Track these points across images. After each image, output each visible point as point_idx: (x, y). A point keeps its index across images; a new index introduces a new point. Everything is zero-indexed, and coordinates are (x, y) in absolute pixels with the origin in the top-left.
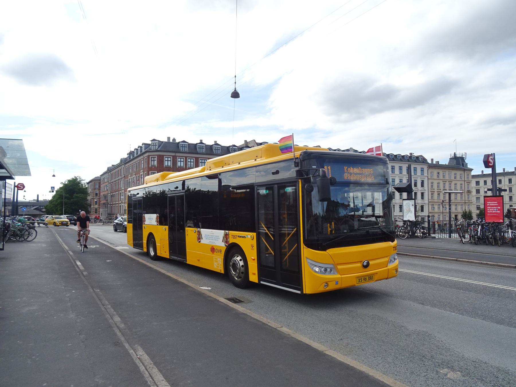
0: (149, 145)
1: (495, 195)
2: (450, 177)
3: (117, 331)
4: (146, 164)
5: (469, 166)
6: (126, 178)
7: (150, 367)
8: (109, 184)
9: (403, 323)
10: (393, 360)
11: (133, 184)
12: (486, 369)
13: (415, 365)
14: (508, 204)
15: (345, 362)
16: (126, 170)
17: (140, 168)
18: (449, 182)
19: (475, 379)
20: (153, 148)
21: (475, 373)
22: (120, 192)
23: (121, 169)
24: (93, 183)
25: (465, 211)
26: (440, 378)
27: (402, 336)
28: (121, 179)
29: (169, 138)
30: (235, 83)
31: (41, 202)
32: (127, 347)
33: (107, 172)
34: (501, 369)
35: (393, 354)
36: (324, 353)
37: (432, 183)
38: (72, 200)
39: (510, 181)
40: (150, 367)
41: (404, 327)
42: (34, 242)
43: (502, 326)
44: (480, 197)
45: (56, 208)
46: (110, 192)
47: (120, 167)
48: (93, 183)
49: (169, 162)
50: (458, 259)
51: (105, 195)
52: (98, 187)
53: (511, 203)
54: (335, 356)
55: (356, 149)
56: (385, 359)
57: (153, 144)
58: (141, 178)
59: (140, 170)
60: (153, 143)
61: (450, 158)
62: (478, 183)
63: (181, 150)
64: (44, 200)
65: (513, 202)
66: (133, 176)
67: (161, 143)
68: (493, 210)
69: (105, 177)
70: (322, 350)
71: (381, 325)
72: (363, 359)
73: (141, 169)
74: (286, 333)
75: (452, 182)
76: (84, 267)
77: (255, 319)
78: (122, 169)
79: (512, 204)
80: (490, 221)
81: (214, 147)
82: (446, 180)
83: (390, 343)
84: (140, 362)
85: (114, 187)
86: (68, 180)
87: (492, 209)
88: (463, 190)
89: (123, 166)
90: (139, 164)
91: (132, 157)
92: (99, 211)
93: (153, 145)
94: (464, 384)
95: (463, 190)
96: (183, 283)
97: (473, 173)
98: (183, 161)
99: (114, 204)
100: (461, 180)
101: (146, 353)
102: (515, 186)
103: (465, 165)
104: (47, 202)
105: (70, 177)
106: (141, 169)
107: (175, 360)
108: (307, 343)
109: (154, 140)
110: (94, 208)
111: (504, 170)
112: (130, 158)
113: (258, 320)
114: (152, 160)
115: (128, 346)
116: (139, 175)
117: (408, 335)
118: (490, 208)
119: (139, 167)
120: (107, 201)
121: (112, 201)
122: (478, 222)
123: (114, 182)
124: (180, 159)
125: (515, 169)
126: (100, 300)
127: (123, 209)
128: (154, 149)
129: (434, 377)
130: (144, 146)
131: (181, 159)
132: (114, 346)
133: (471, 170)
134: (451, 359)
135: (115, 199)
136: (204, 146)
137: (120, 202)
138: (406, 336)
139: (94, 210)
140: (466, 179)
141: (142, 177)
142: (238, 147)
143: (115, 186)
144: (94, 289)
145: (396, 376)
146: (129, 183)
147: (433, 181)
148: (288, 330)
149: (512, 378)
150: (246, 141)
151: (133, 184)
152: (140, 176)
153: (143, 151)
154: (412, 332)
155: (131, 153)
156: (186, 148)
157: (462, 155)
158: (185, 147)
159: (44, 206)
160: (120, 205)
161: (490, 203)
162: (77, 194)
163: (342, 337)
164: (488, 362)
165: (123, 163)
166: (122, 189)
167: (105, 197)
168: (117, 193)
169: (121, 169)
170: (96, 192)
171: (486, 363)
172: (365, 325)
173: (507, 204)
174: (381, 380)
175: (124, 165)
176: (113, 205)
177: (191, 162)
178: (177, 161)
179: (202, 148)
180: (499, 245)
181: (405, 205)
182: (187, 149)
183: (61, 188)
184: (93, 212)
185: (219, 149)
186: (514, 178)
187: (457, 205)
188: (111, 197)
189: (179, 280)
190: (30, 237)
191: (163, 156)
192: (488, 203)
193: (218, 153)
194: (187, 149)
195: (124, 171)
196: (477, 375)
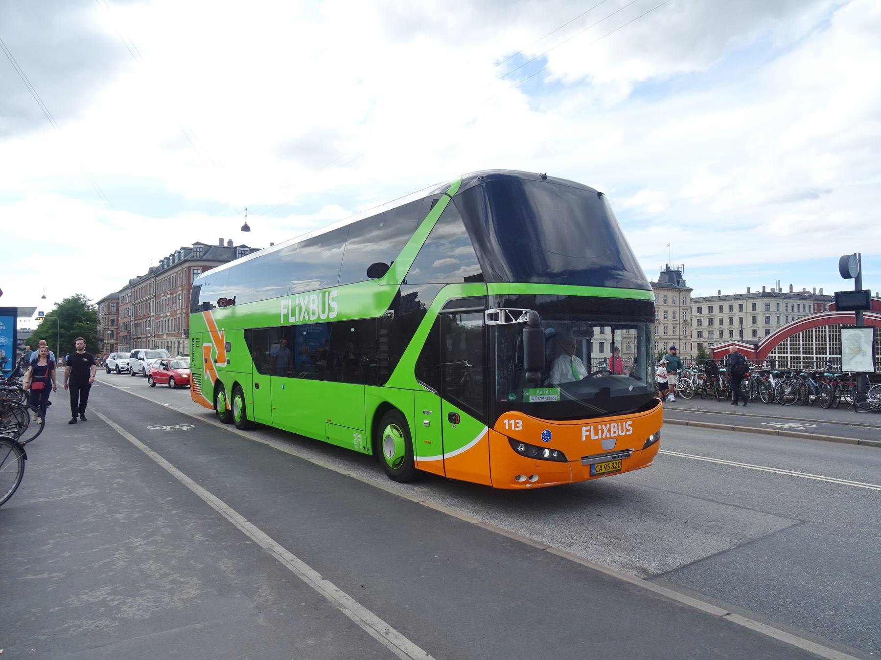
0: (190, 249)
5: (688, 285)
6: (157, 298)
11: (167, 309)
22: (149, 319)
24: (107, 303)
28: (150, 299)
29: (222, 240)
33: (128, 287)
38: (71, 331)
44: (713, 331)
48: (107, 303)
50: (690, 422)
58: (178, 300)
60: (197, 248)
62: (711, 309)
67: (209, 248)
73: (178, 286)
79: (702, 342)
86: (65, 300)
88: (677, 321)
89: (153, 280)
93: (197, 251)
95: (677, 321)
96: (436, 512)
97: (693, 295)
99: (139, 338)
100: (665, 306)
104: (26, 332)
105: (69, 294)
106: (178, 286)
109: (197, 244)
110: (108, 344)
111: (804, 289)
112: (163, 269)
114: (194, 274)
116: (175, 295)
119: (177, 283)
120: (129, 332)
121: (136, 333)
123: (140, 303)
133: (690, 290)
135: (141, 330)
137: (149, 335)
139: (108, 347)
140: (681, 304)
143: (142, 310)
151: (167, 309)
160: (148, 339)
167: (126, 326)
168: (143, 320)
170: (112, 318)
176: (139, 340)
181: (845, 340)
183: (54, 312)
184: (107, 351)
187: (668, 343)
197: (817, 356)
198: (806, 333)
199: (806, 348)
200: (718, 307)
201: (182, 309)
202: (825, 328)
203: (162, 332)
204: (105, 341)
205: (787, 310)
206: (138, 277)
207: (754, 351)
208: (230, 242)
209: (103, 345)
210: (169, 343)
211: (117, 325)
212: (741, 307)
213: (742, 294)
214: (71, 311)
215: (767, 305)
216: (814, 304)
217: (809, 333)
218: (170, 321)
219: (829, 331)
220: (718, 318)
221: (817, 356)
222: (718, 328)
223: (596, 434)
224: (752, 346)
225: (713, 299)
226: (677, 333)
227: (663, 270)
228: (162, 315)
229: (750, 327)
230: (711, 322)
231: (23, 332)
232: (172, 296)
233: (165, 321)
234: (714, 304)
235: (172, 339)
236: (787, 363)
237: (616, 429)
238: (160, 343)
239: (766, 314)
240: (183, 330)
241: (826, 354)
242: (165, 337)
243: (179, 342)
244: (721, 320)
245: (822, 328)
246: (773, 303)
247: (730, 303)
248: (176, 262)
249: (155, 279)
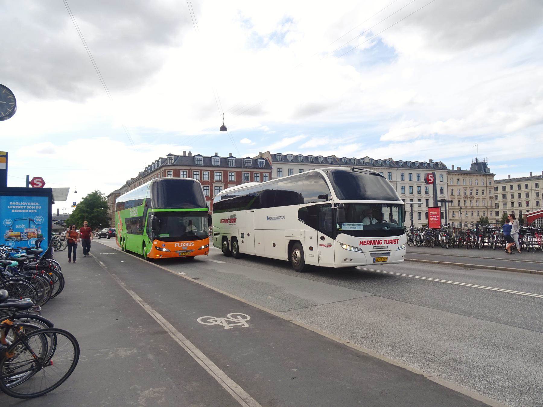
0: (166, 159)
1: (435, 206)
2: (471, 183)
5: (491, 172)
14: (518, 209)
18: (470, 188)
20: (168, 162)
25: (482, 218)
29: (184, 152)
30: (223, 119)
31: (62, 216)
33: (126, 186)
37: (452, 190)
39: (537, 185)
42: (65, 251)
44: (506, 203)
45: (78, 222)
53: (497, 210)
54: (227, 294)
55: (372, 158)
61: (472, 163)
62: (504, 188)
63: (197, 164)
64: (64, 214)
67: (177, 157)
68: (434, 218)
75: (473, 188)
82: (466, 187)
86: (89, 194)
97: (496, 178)
102: (542, 190)
103: (487, 170)
104: (67, 216)
105: (91, 191)
109: (170, 155)
114: (168, 174)
125: (542, 173)
128: (170, 163)
133: (494, 175)
136: (219, 159)
147: (459, 188)
150: (260, 153)
156: (201, 161)
158: (200, 160)
159: (65, 220)
161: (432, 212)
162: (98, 208)
173: (534, 209)
177: (206, 175)
178: (193, 174)
179: (217, 161)
180: (479, 248)
182: (202, 163)
183: (81, 203)
186: (541, 183)
190: (62, 247)
191: (179, 170)
192: (431, 212)
194: (202, 163)
200: (525, 185)
204: (112, 220)
206: (132, 179)
208: (190, 153)
209: (111, 222)
212: (527, 186)
213: (505, 180)
214: (91, 201)
220: (525, 193)
222: (518, 200)
223: (180, 245)
225: (506, 181)
226: (486, 205)
227: (473, 162)
229: (534, 200)
230: (504, 197)
231: (65, 216)
234: (498, 185)
237: (187, 244)
239: (503, 193)
244: (512, 196)
247: (519, 183)
248: (149, 172)
249: (143, 180)
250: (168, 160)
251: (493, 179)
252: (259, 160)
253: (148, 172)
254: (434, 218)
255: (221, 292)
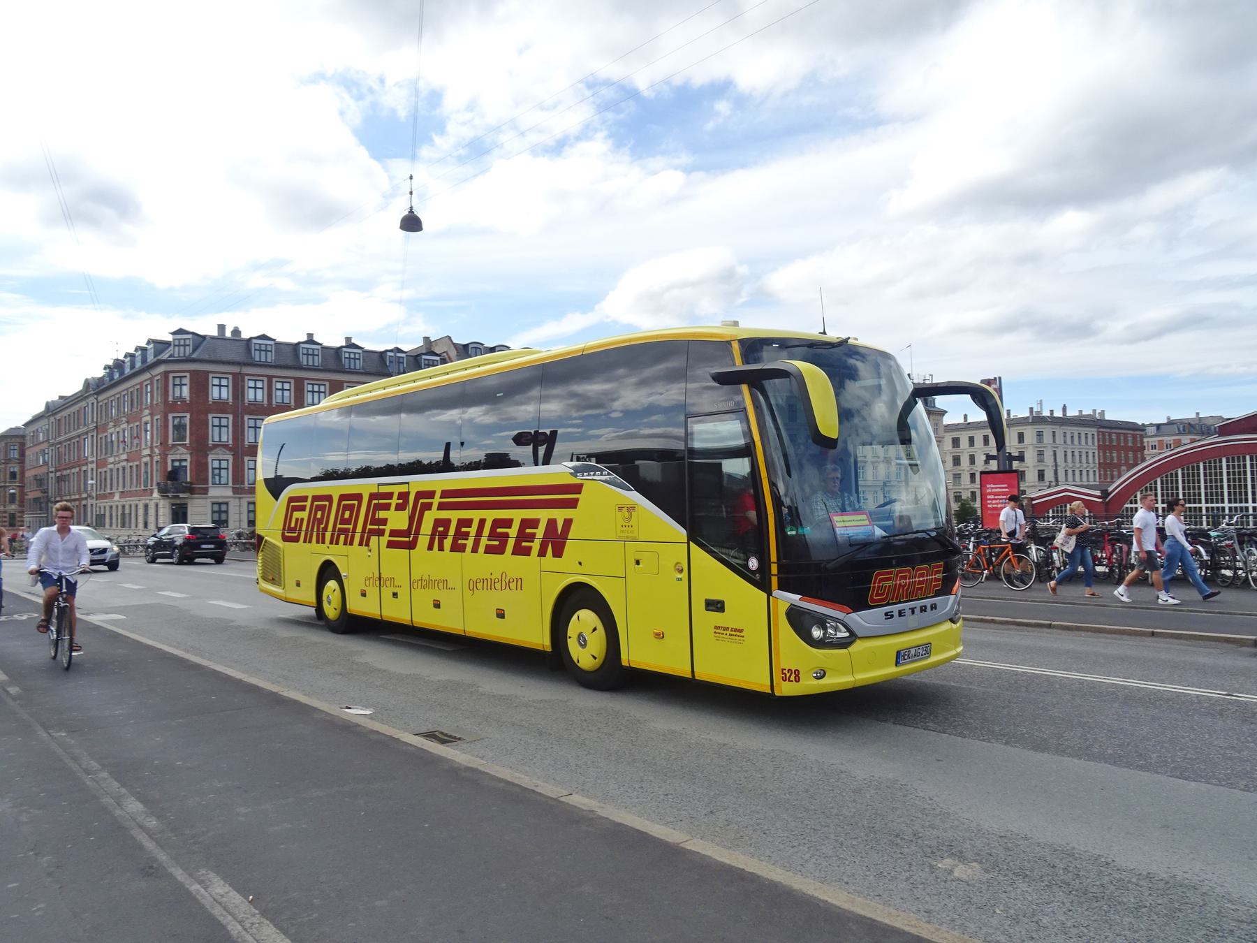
0: (168, 344)
1: (1002, 469)
3: (141, 837)
4: (159, 392)
6: (99, 430)
7: (252, 924)
8: (51, 448)
9: (842, 764)
10: (834, 850)
12: (1028, 850)
13: (883, 856)
14: (968, 489)
15: (733, 864)
16: (101, 411)
17: (142, 403)
19: (1010, 875)
20: (177, 352)
21: (1008, 863)
22: (84, 468)
23: (85, 407)
26: (939, 880)
27: (844, 794)
28: (87, 433)
32: (179, 878)
34: (1058, 848)
35: (832, 836)
36: (682, 848)
40: (252, 924)
41: (845, 772)
43: (1046, 754)
46: (53, 469)
47: (84, 402)
49: (224, 390)
50: (1053, 623)
51: (38, 478)
52: (16, 456)
54: (708, 853)
56: (818, 848)
57: (177, 343)
58: (143, 432)
59: (141, 411)
62: (956, 442)
65: (1027, 484)
66: (122, 427)
69: (37, 430)
70: (676, 841)
71: (794, 772)
72: (768, 853)
73: (144, 407)
74: (585, 809)
76: (7, 675)
77: (500, 780)
78: (88, 406)
80: (992, 527)
81: (303, 348)
83: (822, 811)
84: (225, 913)
85: (65, 455)
87: (996, 499)
89: (92, 400)
90: (137, 396)
91: (116, 376)
92: (19, 519)
93: (179, 346)
94: (991, 888)
98: (227, 386)
101: (233, 888)
106: (144, 407)
107: (316, 899)
108: (637, 828)
109: (180, 331)
110: (5, 512)
111: (1081, 411)
112: (111, 378)
113: (508, 783)
114: (174, 385)
115: (182, 874)
117: (858, 791)
118: (992, 497)
119: (140, 402)
120: (46, 492)
122: (969, 528)
123: (66, 440)
124: (254, 382)
126: (75, 759)
127: (94, 513)
128: (182, 355)
129: (927, 880)
130: (152, 346)
131: (319, 387)
132: (143, 877)
134: (955, 835)
137: (84, 495)
138: (852, 794)
139: (5, 517)
141: (149, 428)
142: (407, 354)
143: (69, 453)
144: (50, 731)
145: (847, 886)
146: (109, 445)
148: (586, 800)
149: (1081, 864)
150: (426, 339)
152: (141, 425)
153: (149, 360)
154: (866, 782)
155: (118, 364)
157: (924, 380)
158: (313, 355)
160: (84, 502)
161: (992, 486)
163: (713, 807)
164: (1030, 836)
165: (92, 392)
166: (90, 459)
167: (40, 481)
168: (73, 470)
169: (85, 407)
170: (12, 470)
171: (1026, 838)
172: (760, 776)
174: (822, 898)
175: (95, 396)
185: (316, 355)
188: (58, 482)
189: (285, 694)
191: (207, 373)
192: (988, 486)
193: (355, 369)
195: (95, 413)
196: (1013, 867)
197: (1230, 505)
198: (1188, 470)
199: (1189, 493)
200: (968, 439)
201: (151, 448)
202: (1244, 460)
203: (111, 489)
205: (1065, 442)
206: (61, 397)
207: (1100, 500)
208: (236, 332)
210: (127, 507)
211: (22, 480)
213: (958, 424)
215: (1040, 435)
216: (1098, 432)
217: (1193, 470)
218: (128, 470)
219: (1228, 467)
221: (1230, 505)
224: (1098, 493)
228: (111, 460)
232: (131, 425)
233: (118, 469)
234: (975, 434)
235: (133, 501)
236: (1201, 517)
238: (107, 509)
240: (155, 483)
241: (1223, 502)
242: (117, 497)
243: (146, 506)
245: (1215, 462)
246: (1047, 431)
248: (115, 378)
250: (175, 346)
251: (942, 422)
252: (424, 357)
253: (113, 379)
254: (997, 501)
255: (776, 874)
